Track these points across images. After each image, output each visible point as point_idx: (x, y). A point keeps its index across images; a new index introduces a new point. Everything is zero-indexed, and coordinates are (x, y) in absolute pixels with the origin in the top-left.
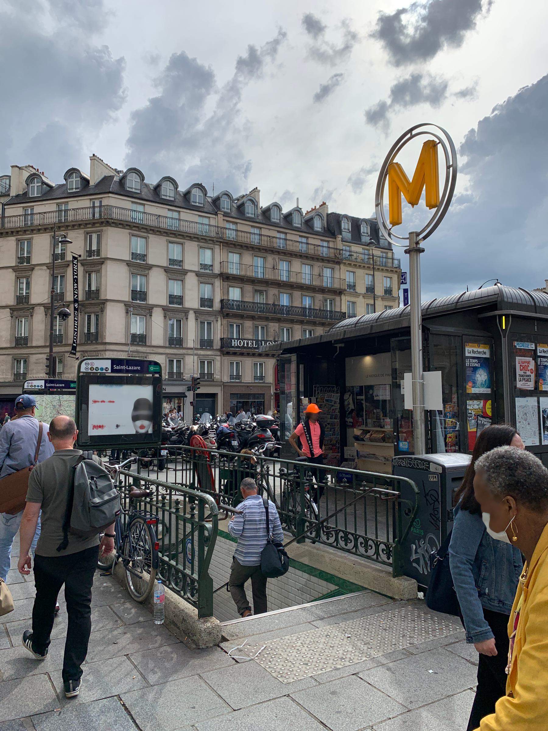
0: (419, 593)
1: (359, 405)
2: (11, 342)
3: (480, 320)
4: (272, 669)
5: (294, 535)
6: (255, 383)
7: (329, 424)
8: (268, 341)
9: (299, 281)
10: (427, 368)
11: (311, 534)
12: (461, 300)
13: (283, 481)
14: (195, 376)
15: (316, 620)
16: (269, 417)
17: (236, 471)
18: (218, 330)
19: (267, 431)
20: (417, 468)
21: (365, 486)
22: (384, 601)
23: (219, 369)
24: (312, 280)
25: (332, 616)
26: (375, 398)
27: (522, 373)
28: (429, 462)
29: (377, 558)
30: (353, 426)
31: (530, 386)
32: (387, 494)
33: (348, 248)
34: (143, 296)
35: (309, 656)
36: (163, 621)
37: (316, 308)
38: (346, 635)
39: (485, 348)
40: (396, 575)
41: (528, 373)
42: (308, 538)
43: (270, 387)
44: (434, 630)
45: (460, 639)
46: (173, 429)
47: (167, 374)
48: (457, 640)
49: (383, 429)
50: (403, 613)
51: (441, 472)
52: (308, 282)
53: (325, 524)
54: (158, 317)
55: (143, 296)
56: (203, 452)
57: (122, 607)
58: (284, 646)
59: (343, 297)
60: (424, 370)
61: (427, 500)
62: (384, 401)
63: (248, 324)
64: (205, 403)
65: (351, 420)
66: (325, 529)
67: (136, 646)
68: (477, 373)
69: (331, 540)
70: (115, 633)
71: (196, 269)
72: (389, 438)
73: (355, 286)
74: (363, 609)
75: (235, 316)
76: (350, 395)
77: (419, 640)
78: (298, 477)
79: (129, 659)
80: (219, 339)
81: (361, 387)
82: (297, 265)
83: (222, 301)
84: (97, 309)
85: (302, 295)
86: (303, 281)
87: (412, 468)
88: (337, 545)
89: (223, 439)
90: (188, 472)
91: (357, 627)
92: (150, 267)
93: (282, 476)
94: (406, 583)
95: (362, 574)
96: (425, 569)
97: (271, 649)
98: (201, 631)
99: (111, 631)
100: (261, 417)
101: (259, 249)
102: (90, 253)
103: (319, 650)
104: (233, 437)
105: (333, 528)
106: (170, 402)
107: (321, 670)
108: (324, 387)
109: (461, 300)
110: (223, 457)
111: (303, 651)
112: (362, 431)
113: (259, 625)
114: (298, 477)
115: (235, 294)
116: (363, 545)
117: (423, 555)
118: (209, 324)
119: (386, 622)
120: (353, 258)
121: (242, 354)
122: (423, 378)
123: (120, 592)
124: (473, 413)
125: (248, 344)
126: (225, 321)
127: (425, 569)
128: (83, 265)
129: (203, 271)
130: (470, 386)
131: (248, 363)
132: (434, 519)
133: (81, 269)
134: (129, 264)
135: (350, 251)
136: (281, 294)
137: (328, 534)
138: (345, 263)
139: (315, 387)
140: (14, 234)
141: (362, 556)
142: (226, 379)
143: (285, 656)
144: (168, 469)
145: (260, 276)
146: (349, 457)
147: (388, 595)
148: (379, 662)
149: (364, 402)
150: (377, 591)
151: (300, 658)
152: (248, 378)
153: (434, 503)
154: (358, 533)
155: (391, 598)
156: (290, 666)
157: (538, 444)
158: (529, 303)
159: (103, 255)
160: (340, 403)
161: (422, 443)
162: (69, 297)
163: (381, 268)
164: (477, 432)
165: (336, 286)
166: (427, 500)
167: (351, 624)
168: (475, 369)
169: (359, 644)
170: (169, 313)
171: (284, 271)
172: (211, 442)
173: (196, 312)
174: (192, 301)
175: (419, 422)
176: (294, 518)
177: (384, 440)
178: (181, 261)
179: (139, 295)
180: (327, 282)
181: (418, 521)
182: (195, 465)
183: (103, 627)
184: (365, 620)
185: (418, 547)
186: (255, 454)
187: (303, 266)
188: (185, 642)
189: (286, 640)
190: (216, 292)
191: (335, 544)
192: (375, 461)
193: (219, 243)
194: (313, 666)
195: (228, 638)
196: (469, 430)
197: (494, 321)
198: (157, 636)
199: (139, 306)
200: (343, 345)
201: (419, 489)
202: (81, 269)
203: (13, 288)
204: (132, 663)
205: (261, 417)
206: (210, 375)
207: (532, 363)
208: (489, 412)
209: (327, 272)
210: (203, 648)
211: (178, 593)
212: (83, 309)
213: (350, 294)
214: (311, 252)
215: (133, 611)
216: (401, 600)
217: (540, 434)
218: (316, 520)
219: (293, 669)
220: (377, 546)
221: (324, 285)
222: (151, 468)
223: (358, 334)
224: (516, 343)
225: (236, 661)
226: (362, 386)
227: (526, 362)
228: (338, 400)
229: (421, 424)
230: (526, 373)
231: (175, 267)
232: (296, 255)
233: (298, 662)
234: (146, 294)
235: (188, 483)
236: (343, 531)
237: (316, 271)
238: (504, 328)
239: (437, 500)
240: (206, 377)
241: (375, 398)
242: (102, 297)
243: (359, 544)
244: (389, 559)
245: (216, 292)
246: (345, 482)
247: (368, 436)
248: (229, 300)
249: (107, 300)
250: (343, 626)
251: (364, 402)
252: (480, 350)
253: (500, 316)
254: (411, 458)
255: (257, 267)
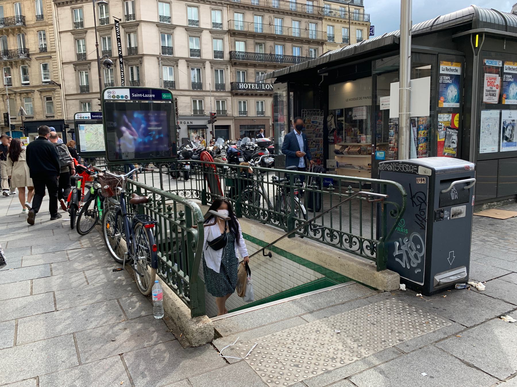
0: (401, 285)
1: (339, 125)
2: (77, 89)
3: (454, 40)
4: (262, 372)
5: (286, 231)
6: (257, 117)
7: (314, 141)
8: (267, 84)
9: (290, 35)
10: (416, 74)
11: (300, 230)
12: (435, 23)
13: (275, 186)
14: (213, 112)
15: (306, 314)
16: (267, 139)
17: (236, 179)
18: (229, 76)
19: (265, 150)
20: (404, 172)
21: (350, 190)
22: (369, 292)
23: (231, 107)
24: (300, 33)
25: (321, 309)
26: (354, 119)
27: (488, 88)
28: (417, 165)
29: (361, 253)
30: (334, 143)
31: (495, 100)
32: (373, 197)
33: (328, 6)
34: (170, 51)
35: (300, 355)
36: (163, 316)
37: (304, 56)
38: (336, 330)
39: (456, 65)
40: (380, 268)
41: (494, 88)
42: (298, 233)
43: (269, 119)
44: (421, 324)
45: (449, 334)
46: (195, 150)
47: (192, 111)
48: (446, 336)
49: (359, 144)
50: (388, 305)
51: (430, 174)
52: (297, 35)
53: (313, 222)
54: (182, 66)
55: (170, 51)
56: (211, 165)
57: (129, 301)
58: (275, 344)
59: (324, 46)
60: (412, 78)
61: (413, 201)
62: (361, 121)
63: (251, 71)
64: (223, 131)
65: (333, 138)
66: (312, 227)
67: (133, 343)
68: (449, 89)
69: (318, 236)
70: (116, 328)
71: (210, 27)
72: (365, 151)
73: (334, 37)
74: (349, 301)
75: (241, 64)
76: (332, 117)
77: (408, 336)
78: (288, 184)
79: (122, 359)
80: (229, 83)
81: (342, 110)
82: (288, 21)
83: (230, 53)
84: (137, 62)
85: (293, 46)
86: (293, 35)
87: (400, 171)
88: (323, 240)
89: (233, 157)
90: (201, 181)
91: (345, 321)
92: (174, 27)
93: (274, 182)
94: (390, 277)
95: (346, 266)
96: (408, 264)
97: (263, 348)
98: (193, 332)
99: (112, 327)
100: (260, 140)
101: (258, 9)
102: (128, 17)
103: (310, 348)
104: (240, 155)
105: (320, 226)
106: (196, 132)
107: (312, 373)
108: (310, 111)
109: (435, 23)
110: (233, 170)
111: (294, 349)
112: (341, 147)
113: (252, 319)
114: (288, 184)
115: (240, 47)
116: (348, 241)
117: (406, 251)
118: (222, 71)
119: (373, 315)
120: (333, 14)
121: (247, 95)
122: (410, 85)
123: (130, 285)
124: (443, 125)
125: (251, 86)
126: (233, 69)
127: (408, 264)
128: (123, 27)
129: (215, 29)
130: (442, 101)
131: (252, 102)
132: (419, 219)
133: (122, 31)
134: (158, 25)
135: (330, 9)
136: (276, 46)
137: (315, 231)
138: (326, 19)
139: (303, 111)
140: (69, 4)
141: (346, 250)
142: (236, 114)
143: (276, 356)
144: (191, 179)
145: (259, 31)
146: (330, 167)
147: (372, 286)
148: (369, 363)
149: (344, 122)
150: (361, 282)
151: (291, 358)
152: (252, 113)
153: (421, 204)
154: (343, 231)
155: (375, 289)
156: (281, 368)
157: (497, 151)
158: (501, 23)
159: (138, 19)
160: (323, 124)
161: (406, 149)
162: (116, 54)
163: (354, 22)
164: (444, 142)
165: (319, 37)
166: (413, 201)
167: (339, 318)
168: (448, 85)
169: (349, 341)
170: (191, 63)
171: (279, 25)
172: (223, 159)
173: (211, 62)
174: (207, 54)
175: (404, 130)
176: (286, 217)
177: (359, 152)
178: (198, 21)
179: (167, 50)
180: (312, 35)
181: (402, 221)
182: (205, 176)
183: (106, 322)
184: (353, 313)
185: (401, 244)
186: (251, 165)
187: (293, 22)
188: (180, 339)
189: (277, 337)
190: (224, 45)
191: (321, 239)
192: (354, 168)
193: (226, 5)
194: (304, 368)
195: (221, 334)
196: (439, 140)
197: (468, 39)
198: (154, 332)
199: (168, 59)
200: (327, 74)
201: (406, 191)
202: (122, 31)
203: (73, 48)
204: (124, 364)
205: (260, 140)
206: (224, 111)
207: (499, 79)
208: (456, 124)
209: (312, 27)
210: (196, 347)
211: (175, 290)
212: (127, 62)
213: (330, 44)
214: (299, 10)
215: (138, 304)
216: (385, 291)
217: (499, 142)
218: (305, 219)
219: (284, 371)
220: (361, 243)
221: (310, 37)
222: (179, 179)
223: (342, 57)
224: (486, 61)
225: (227, 362)
226: (343, 109)
227: (493, 78)
228: (322, 122)
229: (406, 132)
230: (492, 88)
231: (194, 26)
232: (287, 13)
233: (289, 363)
234: (172, 49)
235: (201, 190)
236: (329, 229)
237: (303, 26)
238: (477, 46)
239: (424, 202)
240: (222, 113)
241: (354, 119)
242: (140, 52)
243: (344, 240)
244: (372, 254)
245: (224, 45)
246: (331, 187)
247: (346, 150)
248: (236, 52)
249: (144, 55)
250: (332, 320)
251: (344, 122)
252: (453, 68)
253: (474, 35)
254: (398, 162)
255: (257, 23)
